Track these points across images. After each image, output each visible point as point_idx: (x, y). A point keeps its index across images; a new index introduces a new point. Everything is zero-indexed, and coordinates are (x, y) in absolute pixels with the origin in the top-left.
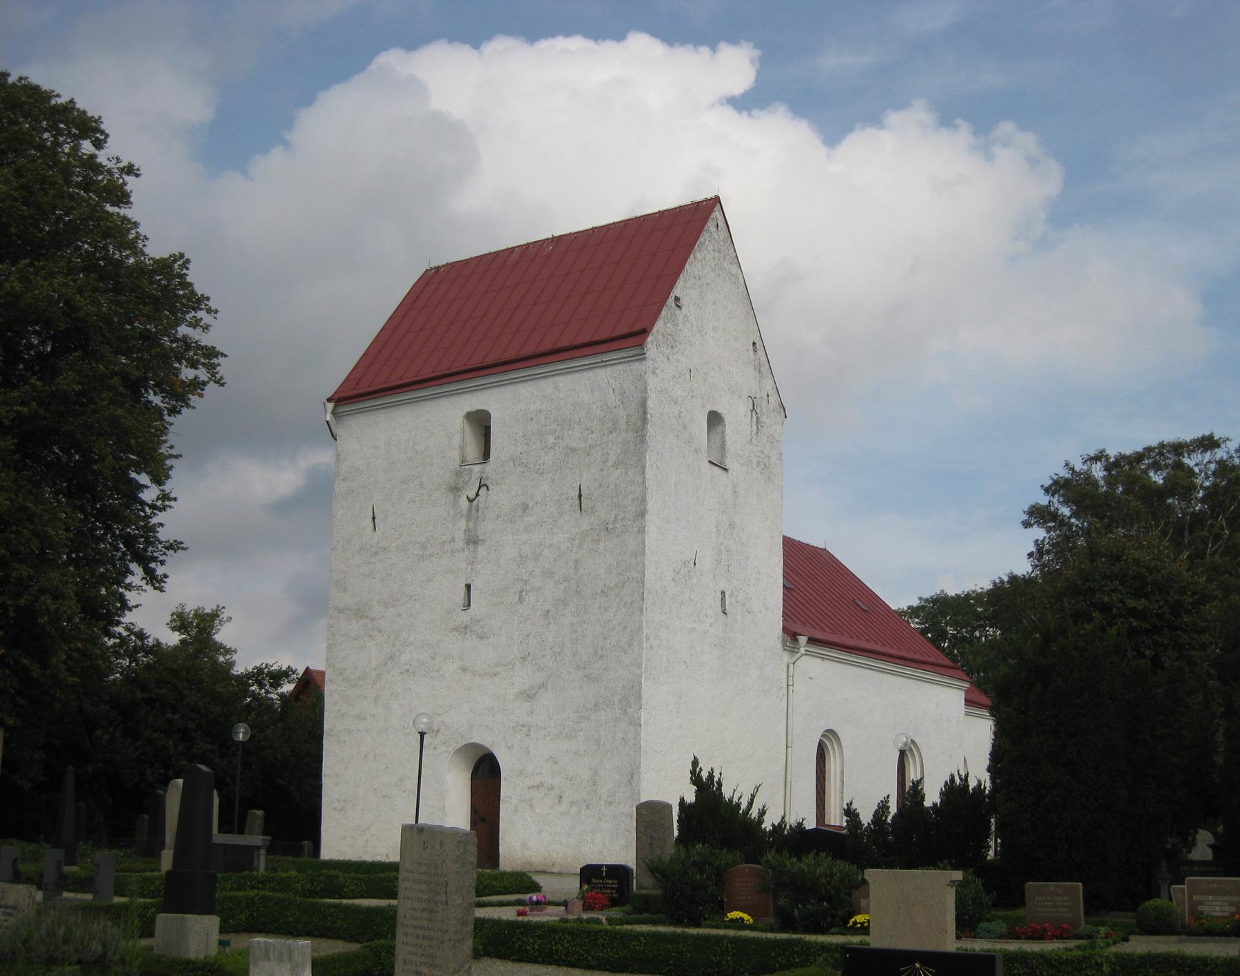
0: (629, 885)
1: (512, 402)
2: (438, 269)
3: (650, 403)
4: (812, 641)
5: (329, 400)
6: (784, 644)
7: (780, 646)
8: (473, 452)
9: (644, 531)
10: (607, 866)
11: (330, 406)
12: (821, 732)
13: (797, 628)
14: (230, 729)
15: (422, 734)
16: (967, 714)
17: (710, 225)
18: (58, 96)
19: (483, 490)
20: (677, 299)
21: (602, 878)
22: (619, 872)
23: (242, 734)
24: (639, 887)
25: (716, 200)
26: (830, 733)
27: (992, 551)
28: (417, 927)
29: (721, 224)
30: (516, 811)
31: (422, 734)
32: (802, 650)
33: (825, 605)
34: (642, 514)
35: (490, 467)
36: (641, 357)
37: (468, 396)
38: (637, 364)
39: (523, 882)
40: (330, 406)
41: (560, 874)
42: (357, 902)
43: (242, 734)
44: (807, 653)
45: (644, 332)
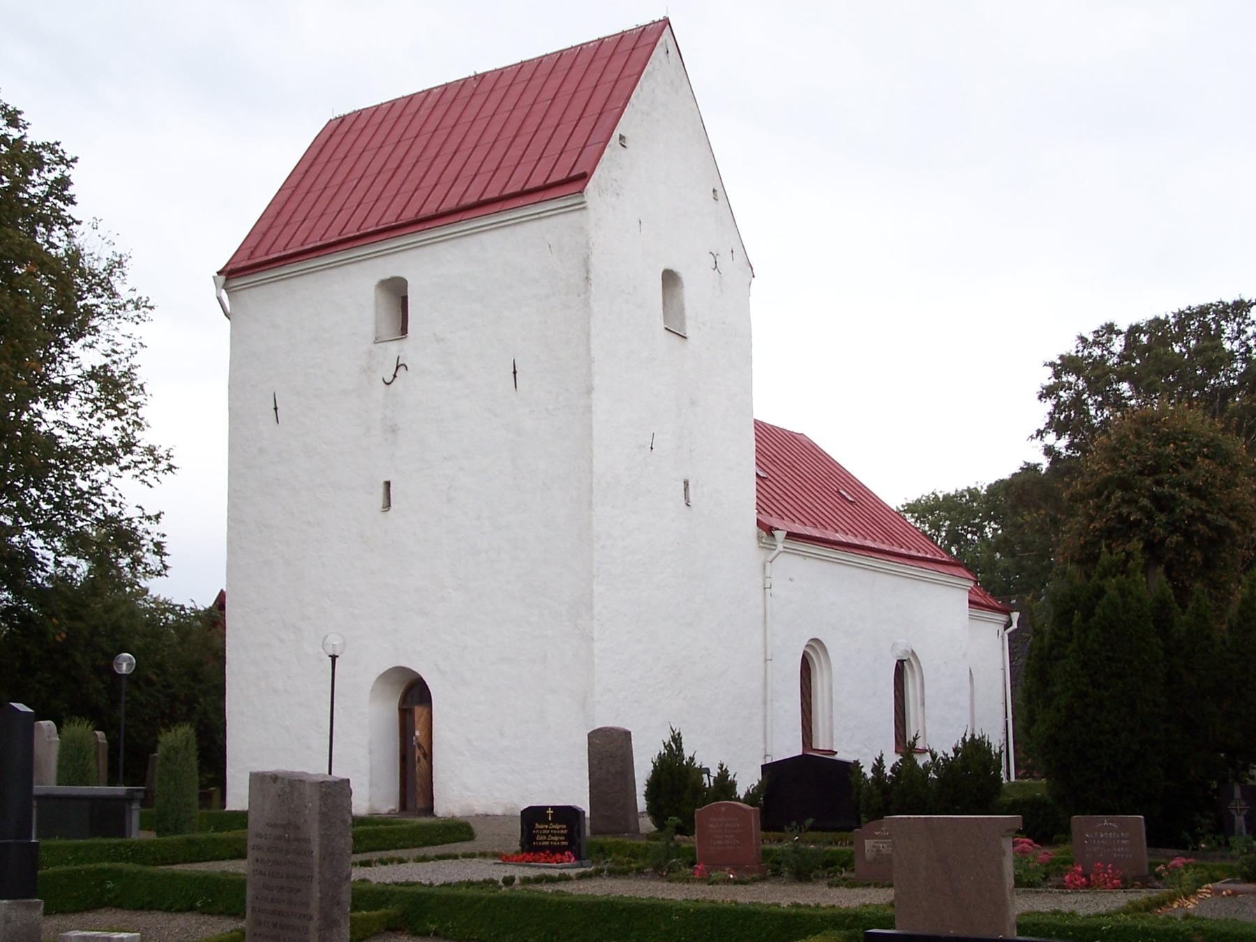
0: (580, 831)
1: (428, 265)
2: (343, 119)
3: (593, 259)
4: (791, 536)
5: (219, 273)
6: (759, 538)
7: (755, 541)
8: (389, 328)
9: (590, 412)
10: (553, 808)
11: (222, 278)
12: (805, 642)
13: (774, 521)
14: (111, 657)
15: (334, 658)
16: (971, 617)
17: (659, 52)
18: (70, 200)
19: (402, 369)
20: (622, 138)
21: (547, 822)
22: (568, 815)
23: (125, 663)
24: (595, 832)
25: (666, 22)
26: (816, 643)
27: (992, 434)
28: (273, 913)
29: (672, 50)
30: (394, 430)
31: (334, 658)
32: (780, 547)
33: (804, 495)
34: (589, 391)
35: (407, 349)
36: (582, 206)
37: (380, 261)
38: (577, 214)
39: (458, 831)
40: (222, 278)
41: (765, 742)
42: (177, 868)
43: (125, 663)
44: (786, 551)
45: (584, 177)
